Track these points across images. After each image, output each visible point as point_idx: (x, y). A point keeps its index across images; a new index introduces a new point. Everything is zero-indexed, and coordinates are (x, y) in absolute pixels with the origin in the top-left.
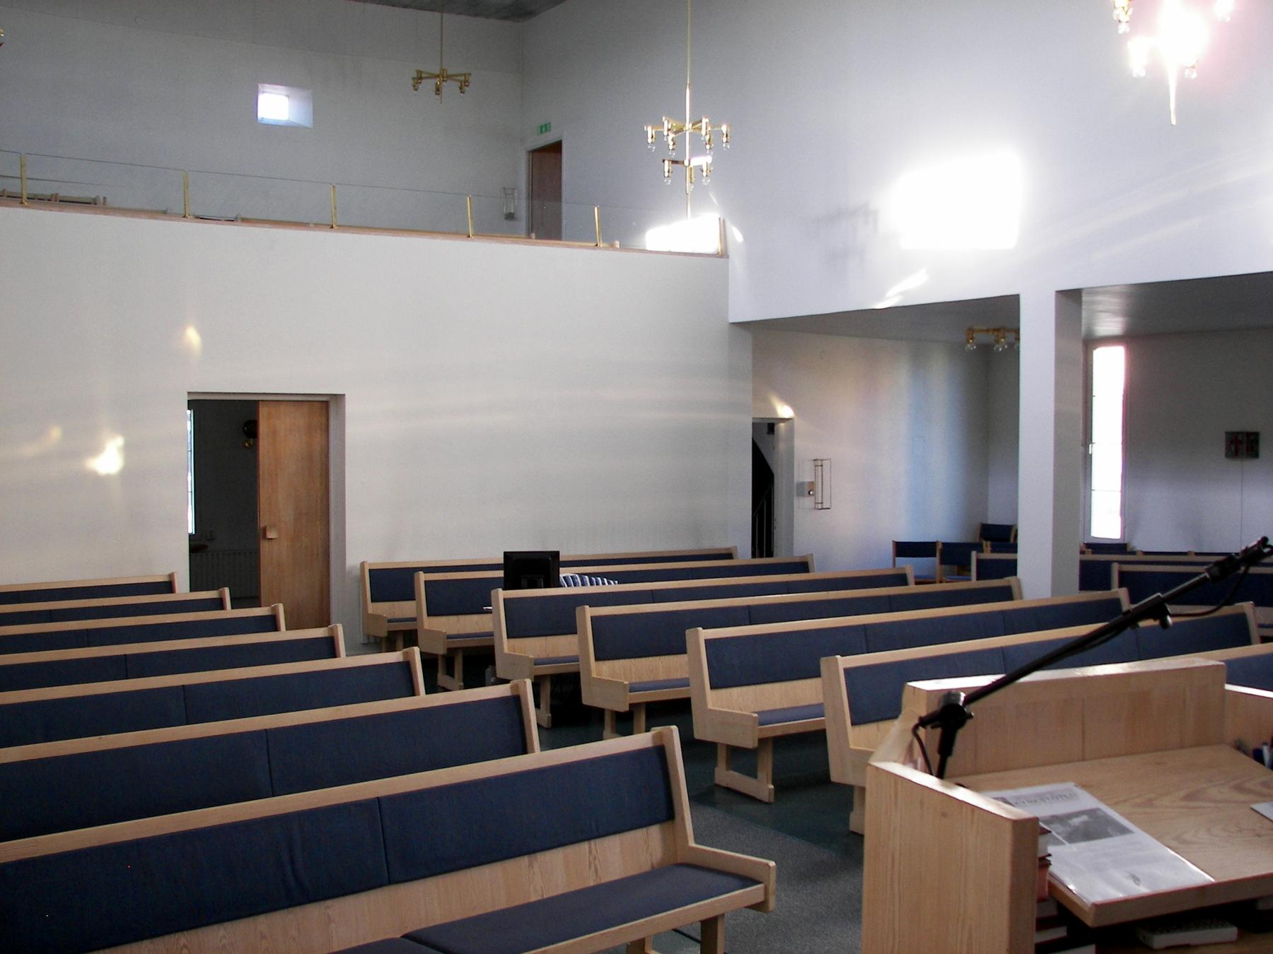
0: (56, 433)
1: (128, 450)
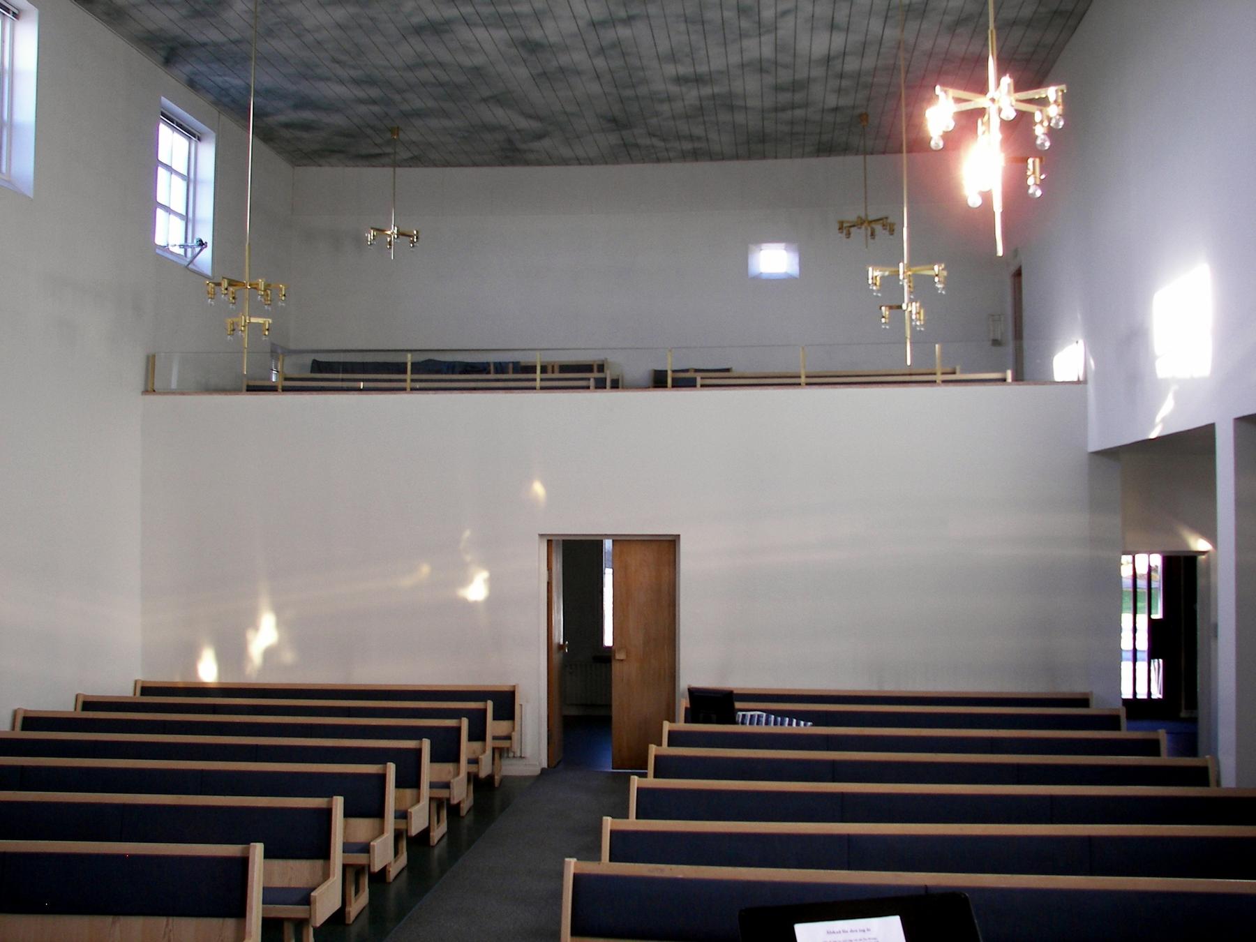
0: (425, 569)
1: (492, 582)
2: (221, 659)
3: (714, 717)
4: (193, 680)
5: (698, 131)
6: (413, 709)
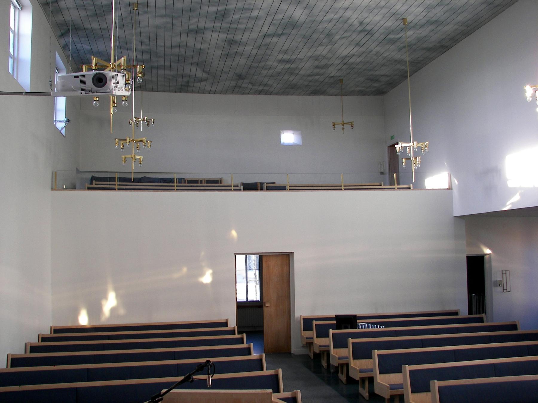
0: (185, 270)
1: (214, 274)
2: (90, 314)
3: (349, 326)
4: (77, 325)
5: (270, 82)
6: (143, 334)
